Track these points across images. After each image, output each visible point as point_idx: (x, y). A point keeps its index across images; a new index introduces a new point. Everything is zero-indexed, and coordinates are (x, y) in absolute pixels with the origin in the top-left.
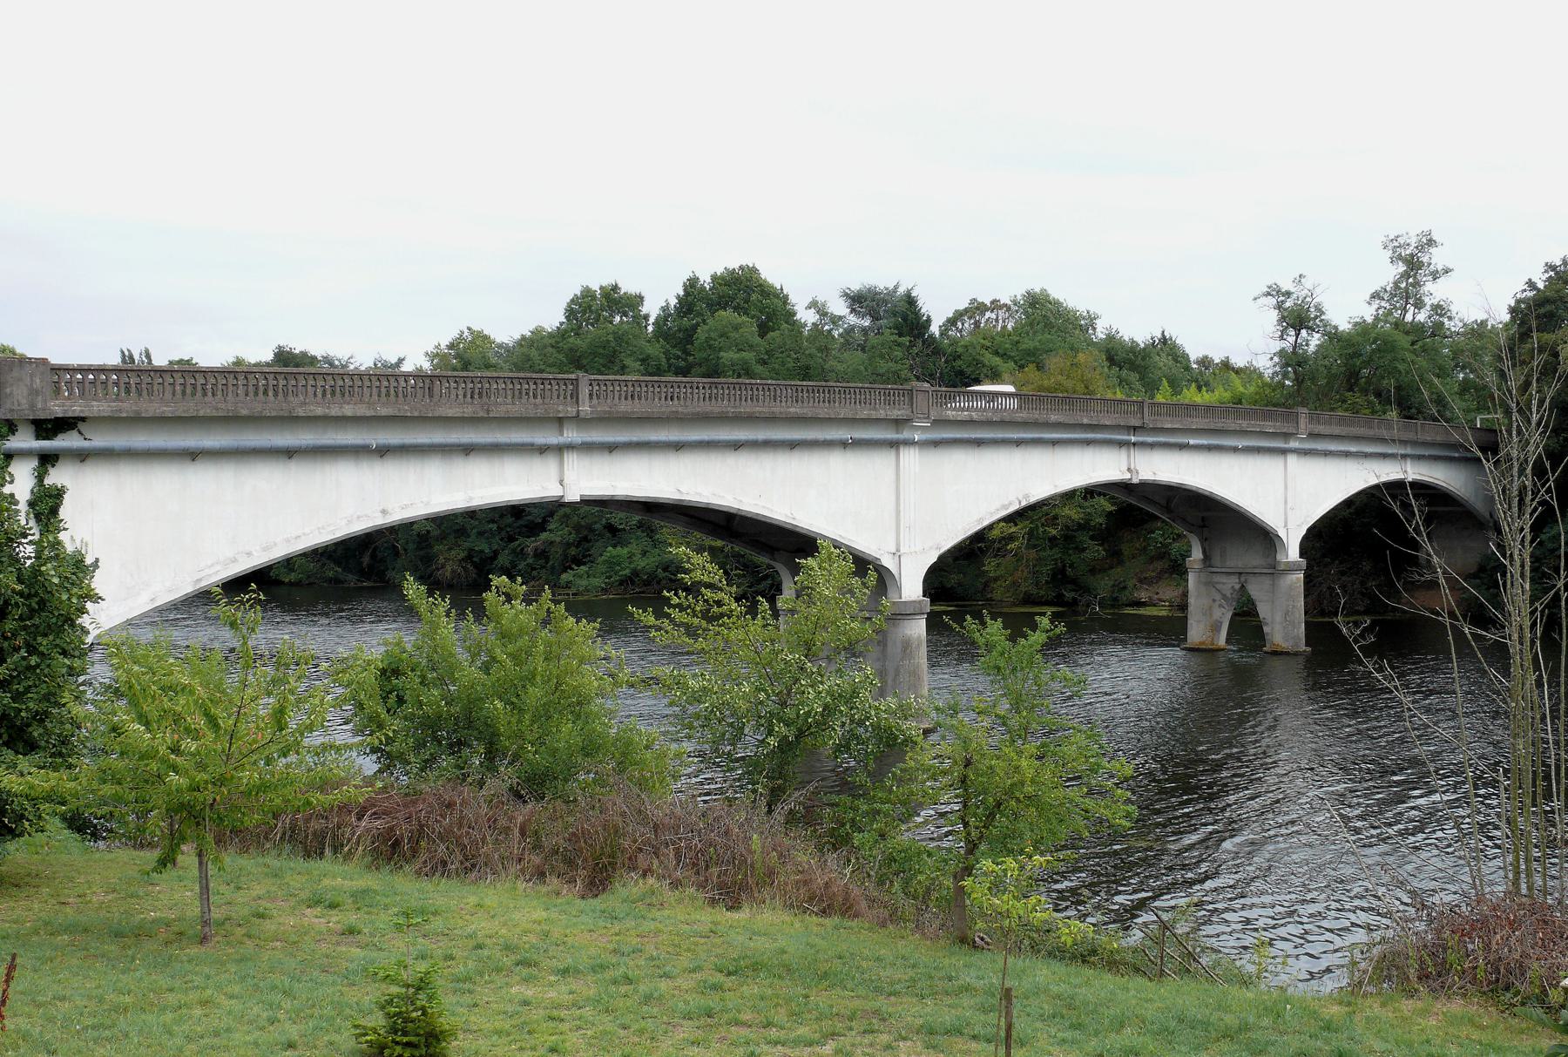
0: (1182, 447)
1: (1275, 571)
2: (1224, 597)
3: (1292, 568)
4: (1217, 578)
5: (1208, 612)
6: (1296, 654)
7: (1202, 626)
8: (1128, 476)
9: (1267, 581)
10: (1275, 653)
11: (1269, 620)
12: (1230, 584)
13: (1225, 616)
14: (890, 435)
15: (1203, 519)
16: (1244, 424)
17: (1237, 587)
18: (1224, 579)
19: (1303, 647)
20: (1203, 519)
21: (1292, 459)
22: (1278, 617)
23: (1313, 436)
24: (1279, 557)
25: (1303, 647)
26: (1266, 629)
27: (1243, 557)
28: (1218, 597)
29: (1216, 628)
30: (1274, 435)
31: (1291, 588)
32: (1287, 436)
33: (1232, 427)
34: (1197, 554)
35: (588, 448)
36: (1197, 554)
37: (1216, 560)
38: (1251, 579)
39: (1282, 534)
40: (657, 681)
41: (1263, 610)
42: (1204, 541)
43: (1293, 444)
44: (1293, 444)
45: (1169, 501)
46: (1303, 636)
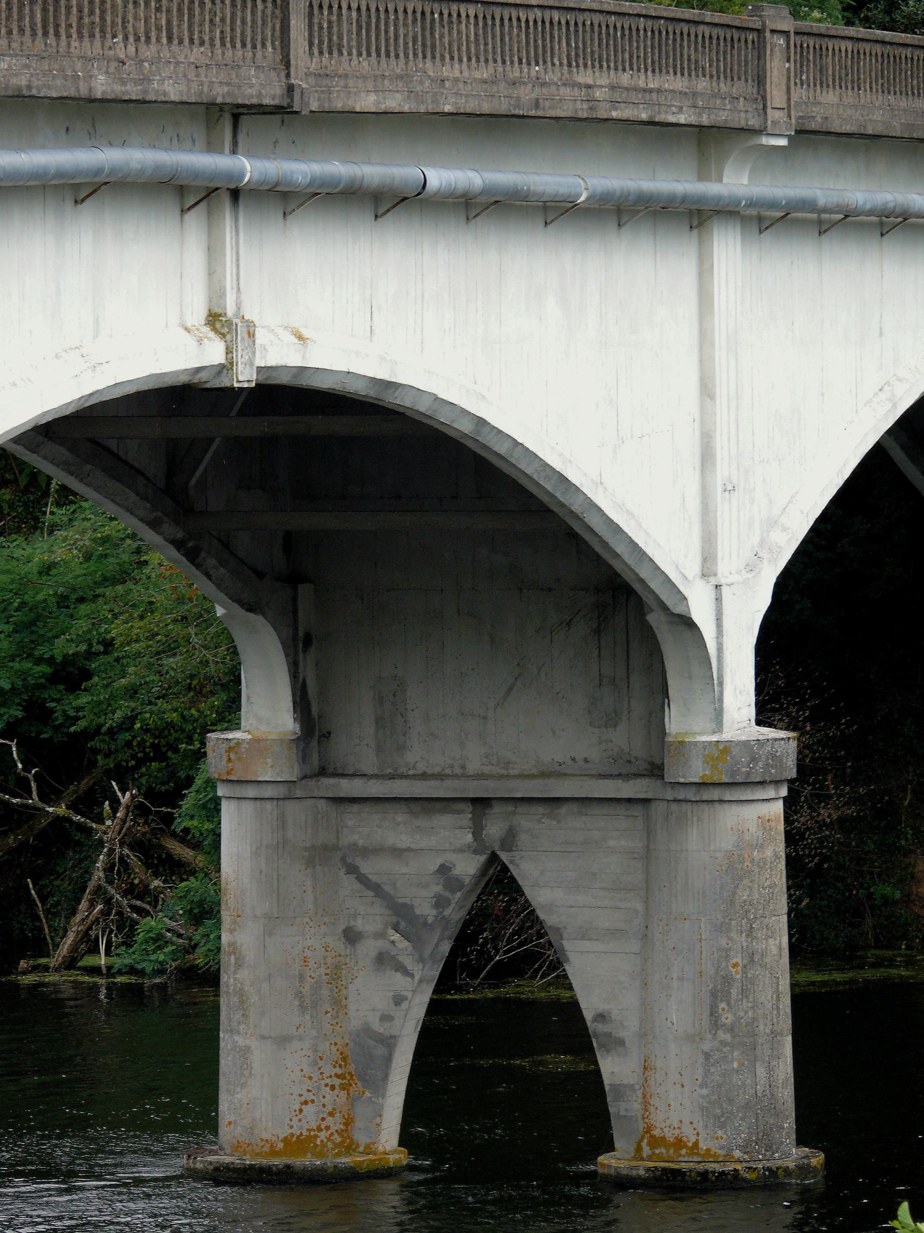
0: (387, 203)
1: (654, 783)
2: (403, 917)
3: (730, 780)
4: (362, 829)
5: (326, 992)
6: (772, 1182)
7: (297, 1060)
8: (213, 353)
9: (617, 836)
10: (675, 1184)
11: (627, 1024)
12: (432, 860)
13: (395, 1003)
14: (673, 180)
15: (289, 542)
16: (599, 86)
17: (468, 867)
18: (396, 831)
19: (791, 1154)
20: (289, 542)
21: (727, 248)
22: (679, 1011)
23: (807, 137)
24: (678, 722)
25: (791, 1154)
26: (613, 1068)
27: (487, 720)
28: (370, 918)
29: (357, 1069)
30: (654, 134)
31: (736, 868)
32: (708, 141)
33: (568, 103)
34: (268, 708)
35: (766, 221)
36: (268, 708)
37: (357, 742)
38: (527, 821)
39: (701, 613)
40: (778, 999)
41: (596, 979)
42: (298, 645)
43: (736, 181)
44: (736, 181)
45: (178, 457)
46: (787, 1095)
